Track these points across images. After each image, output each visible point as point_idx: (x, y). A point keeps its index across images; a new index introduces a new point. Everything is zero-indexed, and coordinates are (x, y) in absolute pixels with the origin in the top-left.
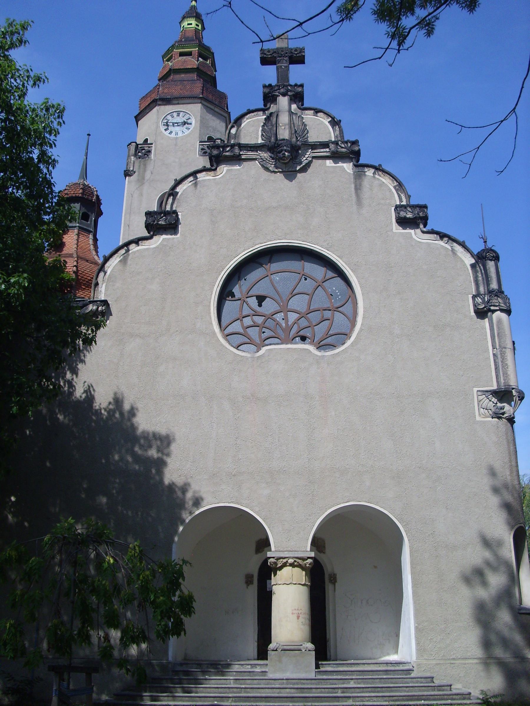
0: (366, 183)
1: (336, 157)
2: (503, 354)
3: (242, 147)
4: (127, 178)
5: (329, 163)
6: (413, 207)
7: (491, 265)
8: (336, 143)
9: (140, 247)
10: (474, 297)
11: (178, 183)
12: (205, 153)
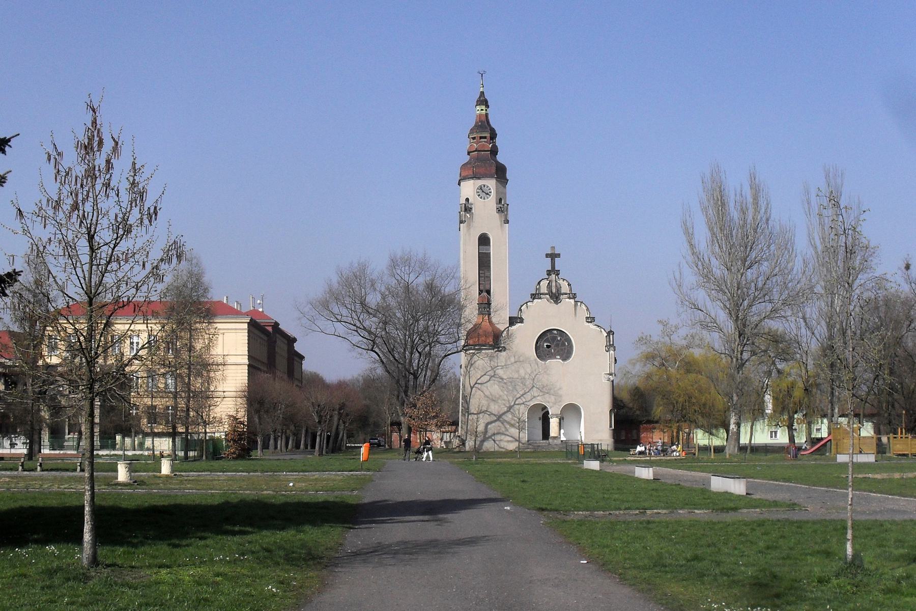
1: (570, 298)
5: (568, 300)
7: (611, 336)
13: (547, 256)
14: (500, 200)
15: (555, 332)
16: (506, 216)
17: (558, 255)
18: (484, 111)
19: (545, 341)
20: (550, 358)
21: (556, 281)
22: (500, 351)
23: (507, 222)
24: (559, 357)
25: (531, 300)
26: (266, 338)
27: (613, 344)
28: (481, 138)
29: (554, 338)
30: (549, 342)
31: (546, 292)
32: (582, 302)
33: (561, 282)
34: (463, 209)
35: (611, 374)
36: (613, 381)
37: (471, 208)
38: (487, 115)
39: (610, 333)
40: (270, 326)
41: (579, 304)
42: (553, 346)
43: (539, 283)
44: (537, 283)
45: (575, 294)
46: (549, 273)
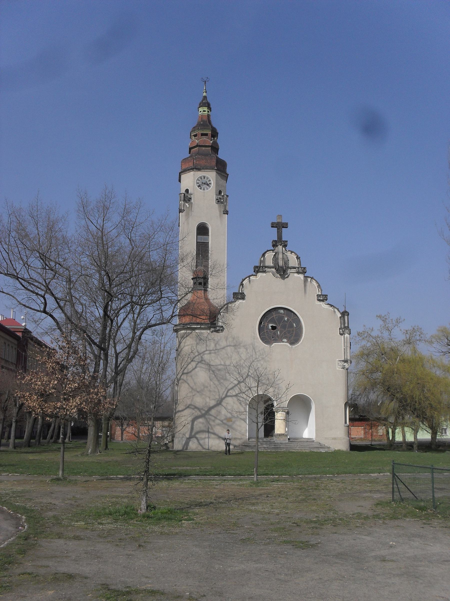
0: (308, 283)
1: (298, 273)
2: (347, 348)
3: (266, 267)
4: (181, 213)
5: (296, 275)
6: (323, 295)
7: (346, 317)
8: (298, 268)
10: (340, 329)
11: (244, 280)
12: (218, 201)
13: (273, 225)
14: (220, 192)
15: (282, 311)
16: (225, 206)
17: (285, 226)
18: (206, 113)
19: (270, 322)
20: (276, 341)
21: (283, 253)
22: (217, 331)
23: (226, 212)
24: (285, 340)
25: (254, 274)
26: (16, 342)
27: (348, 327)
28: (203, 135)
29: (281, 318)
30: (275, 323)
31: (272, 265)
32: (312, 278)
33: (289, 254)
34: (182, 198)
35: (346, 361)
36: (347, 369)
37: (191, 198)
38: (208, 116)
39: (344, 314)
40: (20, 332)
41: (309, 280)
42: (278, 328)
43: (264, 255)
44: (262, 255)
45: (304, 268)
46: (275, 244)
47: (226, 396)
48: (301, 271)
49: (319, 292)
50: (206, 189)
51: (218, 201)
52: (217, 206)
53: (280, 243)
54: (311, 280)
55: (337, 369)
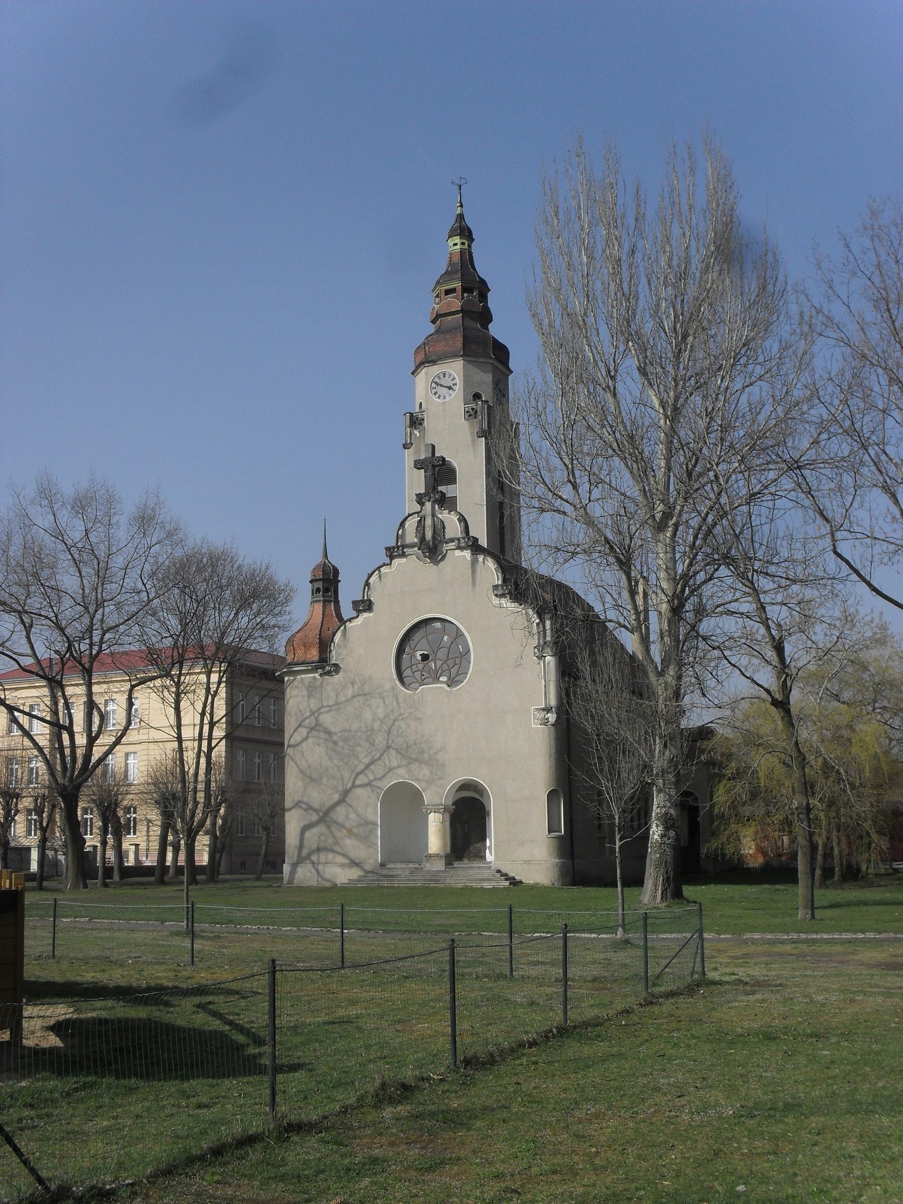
0: (479, 566)
5: (458, 553)
9: (352, 624)
11: (370, 576)
12: (470, 415)
18: (458, 247)
22: (329, 673)
43: (402, 524)
44: (399, 525)
47: (354, 786)
48: (463, 544)
49: (498, 580)
50: (447, 396)
51: (470, 415)
52: (467, 422)
53: (427, 498)
54: (483, 559)
55: (533, 726)
